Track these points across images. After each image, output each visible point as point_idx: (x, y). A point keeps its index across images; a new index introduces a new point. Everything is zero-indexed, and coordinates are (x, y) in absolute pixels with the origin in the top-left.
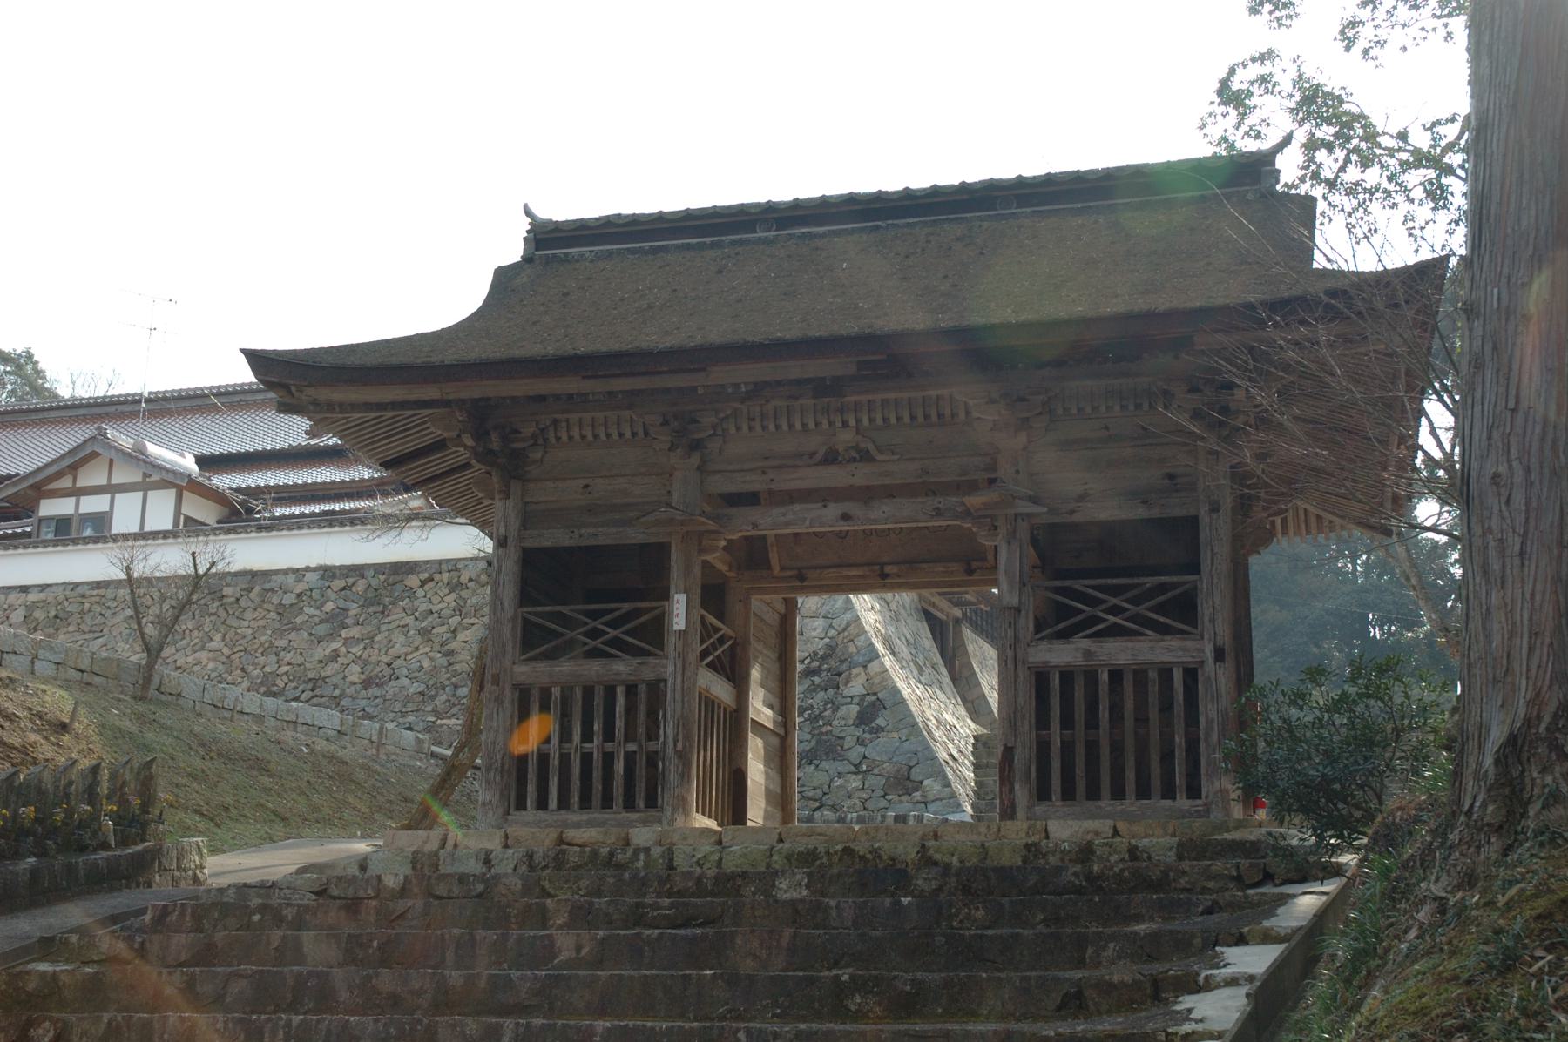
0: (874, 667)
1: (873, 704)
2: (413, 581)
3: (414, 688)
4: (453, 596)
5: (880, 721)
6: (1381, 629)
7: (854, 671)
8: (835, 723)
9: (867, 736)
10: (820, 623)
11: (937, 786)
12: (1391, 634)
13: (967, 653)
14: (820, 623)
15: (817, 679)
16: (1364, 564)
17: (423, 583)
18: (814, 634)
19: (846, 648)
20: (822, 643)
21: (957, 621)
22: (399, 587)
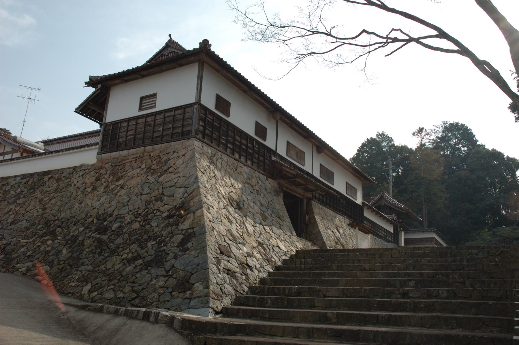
0: (198, 213)
1: (190, 234)
2: (46, 178)
3: (28, 224)
4: (57, 184)
5: (189, 245)
6: (506, 211)
7: (189, 215)
8: (169, 245)
9: (180, 253)
10: (182, 190)
11: (201, 288)
12: (509, 213)
13: (313, 213)
14: (182, 190)
15: (171, 220)
16: (499, 191)
17: (49, 179)
18: (178, 196)
19: (189, 203)
20: (181, 200)
21: (310, 199)
22: (42, 181)
